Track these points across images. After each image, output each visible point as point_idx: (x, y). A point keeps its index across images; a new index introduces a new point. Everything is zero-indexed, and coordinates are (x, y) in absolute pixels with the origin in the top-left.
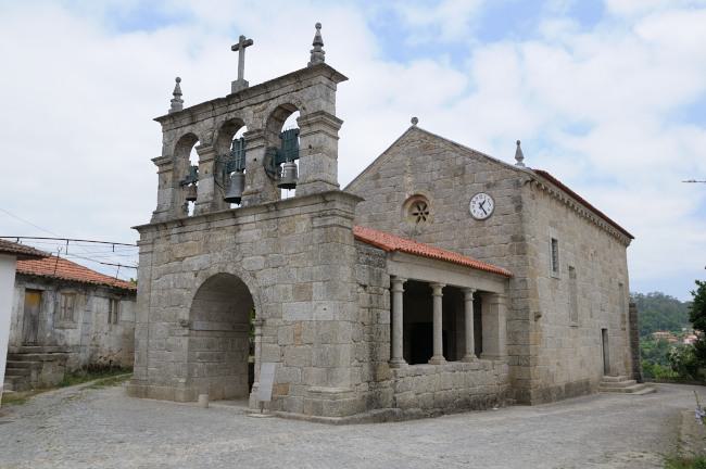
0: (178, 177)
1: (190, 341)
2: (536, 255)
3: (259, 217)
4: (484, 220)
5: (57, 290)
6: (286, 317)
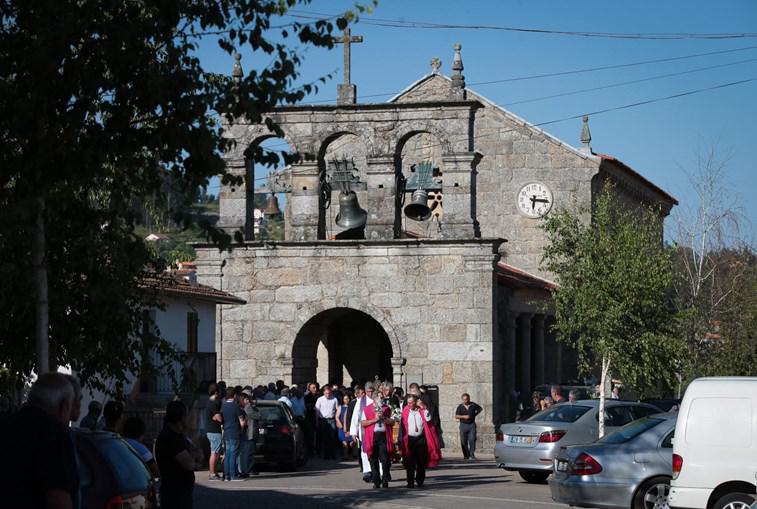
6: (432, 357)
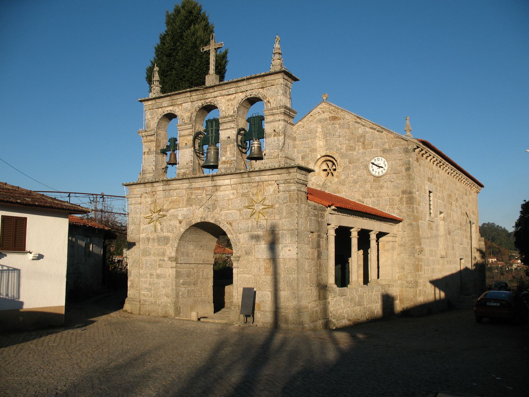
0: (159, 146)
1: (176, 271)
2: (419, 205)
3: (234, 181)
5: (270, 259)
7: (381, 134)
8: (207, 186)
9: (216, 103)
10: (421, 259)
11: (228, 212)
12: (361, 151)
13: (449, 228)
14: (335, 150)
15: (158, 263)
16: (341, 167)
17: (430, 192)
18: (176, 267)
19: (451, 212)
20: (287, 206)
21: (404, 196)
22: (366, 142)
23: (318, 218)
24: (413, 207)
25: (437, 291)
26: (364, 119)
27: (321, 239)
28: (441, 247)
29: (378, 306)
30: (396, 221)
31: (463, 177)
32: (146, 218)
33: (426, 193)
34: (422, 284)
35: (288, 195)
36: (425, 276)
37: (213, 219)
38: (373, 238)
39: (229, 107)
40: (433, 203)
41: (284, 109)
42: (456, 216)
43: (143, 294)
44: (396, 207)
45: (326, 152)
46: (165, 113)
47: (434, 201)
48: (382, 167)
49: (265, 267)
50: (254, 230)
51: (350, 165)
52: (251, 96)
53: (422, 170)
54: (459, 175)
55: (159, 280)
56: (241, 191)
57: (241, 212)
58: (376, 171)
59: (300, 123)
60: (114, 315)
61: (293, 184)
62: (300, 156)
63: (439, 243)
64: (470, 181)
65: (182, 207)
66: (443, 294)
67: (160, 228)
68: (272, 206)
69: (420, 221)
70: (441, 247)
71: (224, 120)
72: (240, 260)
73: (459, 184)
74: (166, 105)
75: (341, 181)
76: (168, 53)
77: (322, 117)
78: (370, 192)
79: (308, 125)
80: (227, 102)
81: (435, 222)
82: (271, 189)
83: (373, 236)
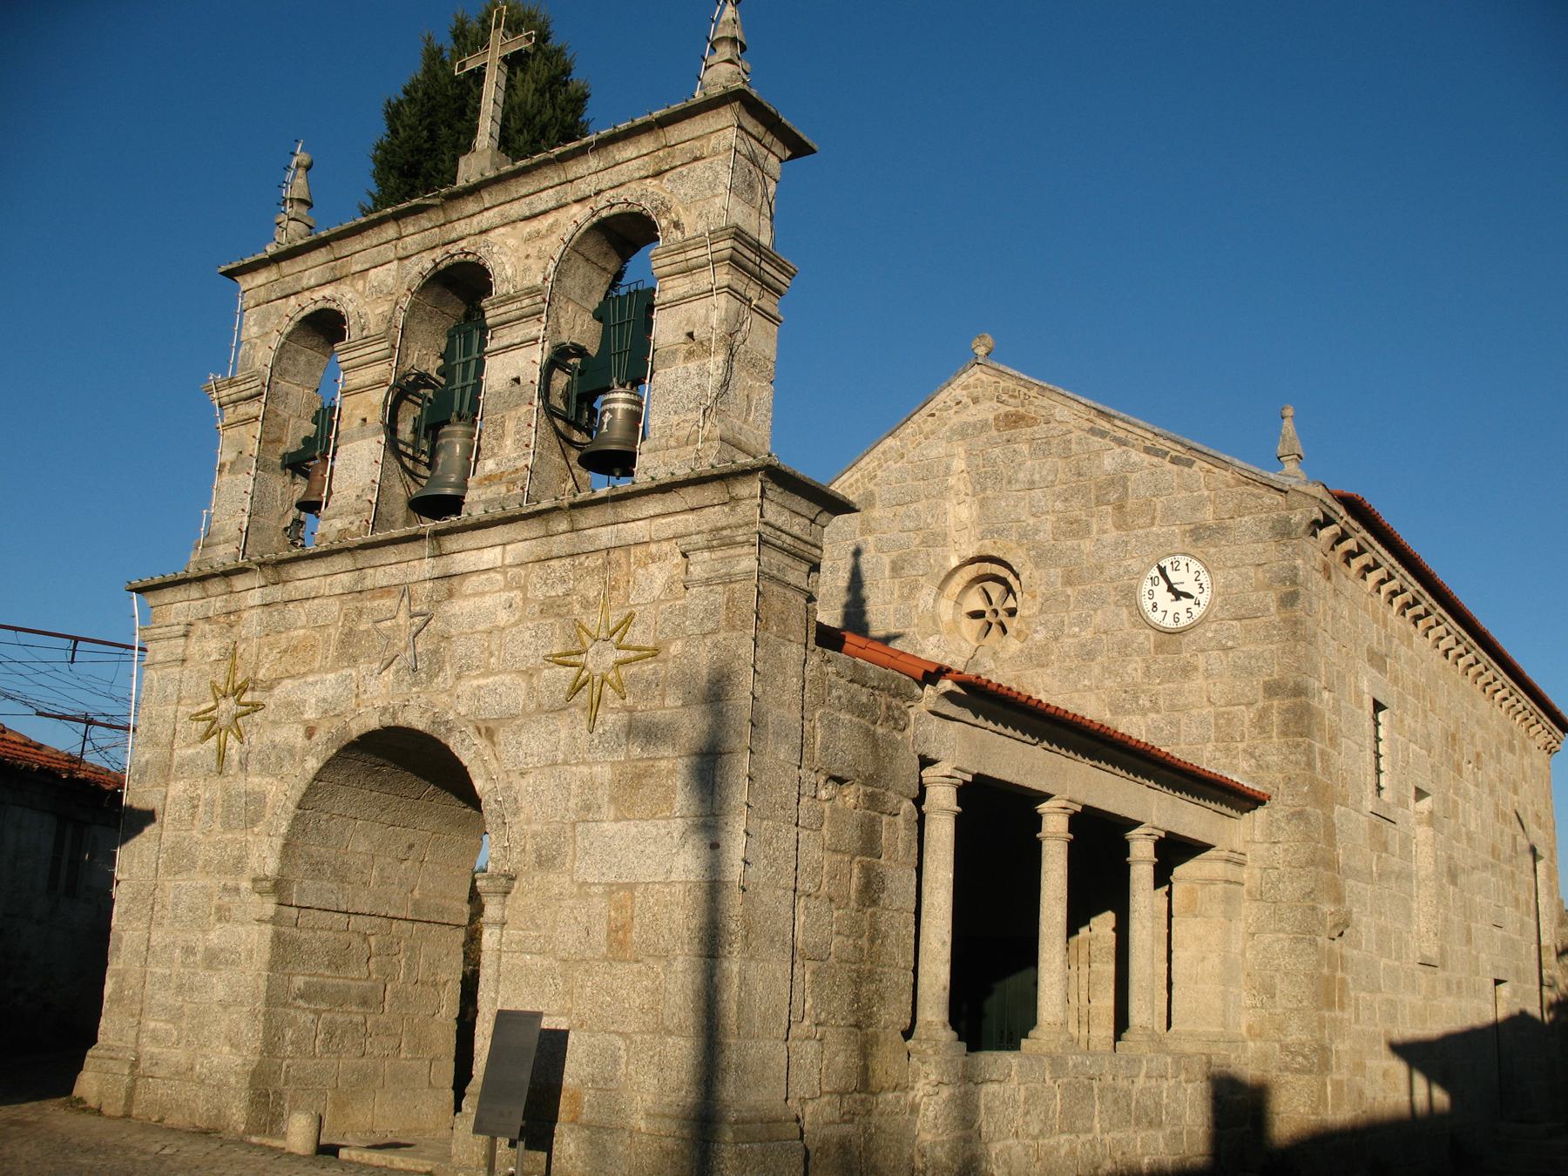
0: (279, 440)
2: (1333, 741)
3: (516, 551)
4: (1182, 632)
7: (1186, 469)
8: (415, 578)
9: (482, 252)
10: (1342, 957)
11: (482, 682)
12: (1112, 535)
13: (1450, 858)
14: (1015, 537)
15: (215, 901)
16: (1034, 597)
17: (1378, 707)
18: (275, 920)
19: (1460, 801)
20: (715, 646)
21: (1276, 703)
22: (1131, 503)
23: (874, 723)
24: (1310, 745)
25: (1420, 1083)
26: (1122, 420)
27: (885, 819)
28: (1422, 924)
29: (1156, 1139)
30: (1241, 800)
31: (1500, 678)
32: (195, 718)
33: (1361, 707)
34: (1346, 1061)
35: (722, 599)
36: (1358, 1027)
37: (427, 715)
38: (1139, 854)
39: (530, 261)
40: (1390, 748)
41: (729, 243)
42: (1476, 817)
43: (154, 1030)
44: (1241, 746)
45: (980, 543)
46: (307, 311)
47: (1393, 741)
48: (1188, 596)
49: (609, 923)
50: (577, 758)
51: (1069, 591)
52: (615, 210)
53: (1346, 613)
54: (1487, 669)
55: (212, 973)
56: (540, 593)
57: (535, 680)
58: (1166, 611)
59: (889, 442)
60: (52, 1113)
61: (746, 549)
62: (886, 560)
63: (1415, 906)
64: (1524, 702)
65: (319, 671)
66: (1441, 1098)
67: (237, 758)
68: (655, 652)
69: (1337, 807)
70: (1422, 924)
71: (502, 310)
72: (513, 892)
73: (1484, 703)
74: (313, 282)
75: (1034, 651)
76: (407, 162)
77: (971, 419)
78: (1143, 692)
79: (918, 450)
80: (522, 248)
81: (1398, 821)
82: (657, 577)
83: (1142, 851)
